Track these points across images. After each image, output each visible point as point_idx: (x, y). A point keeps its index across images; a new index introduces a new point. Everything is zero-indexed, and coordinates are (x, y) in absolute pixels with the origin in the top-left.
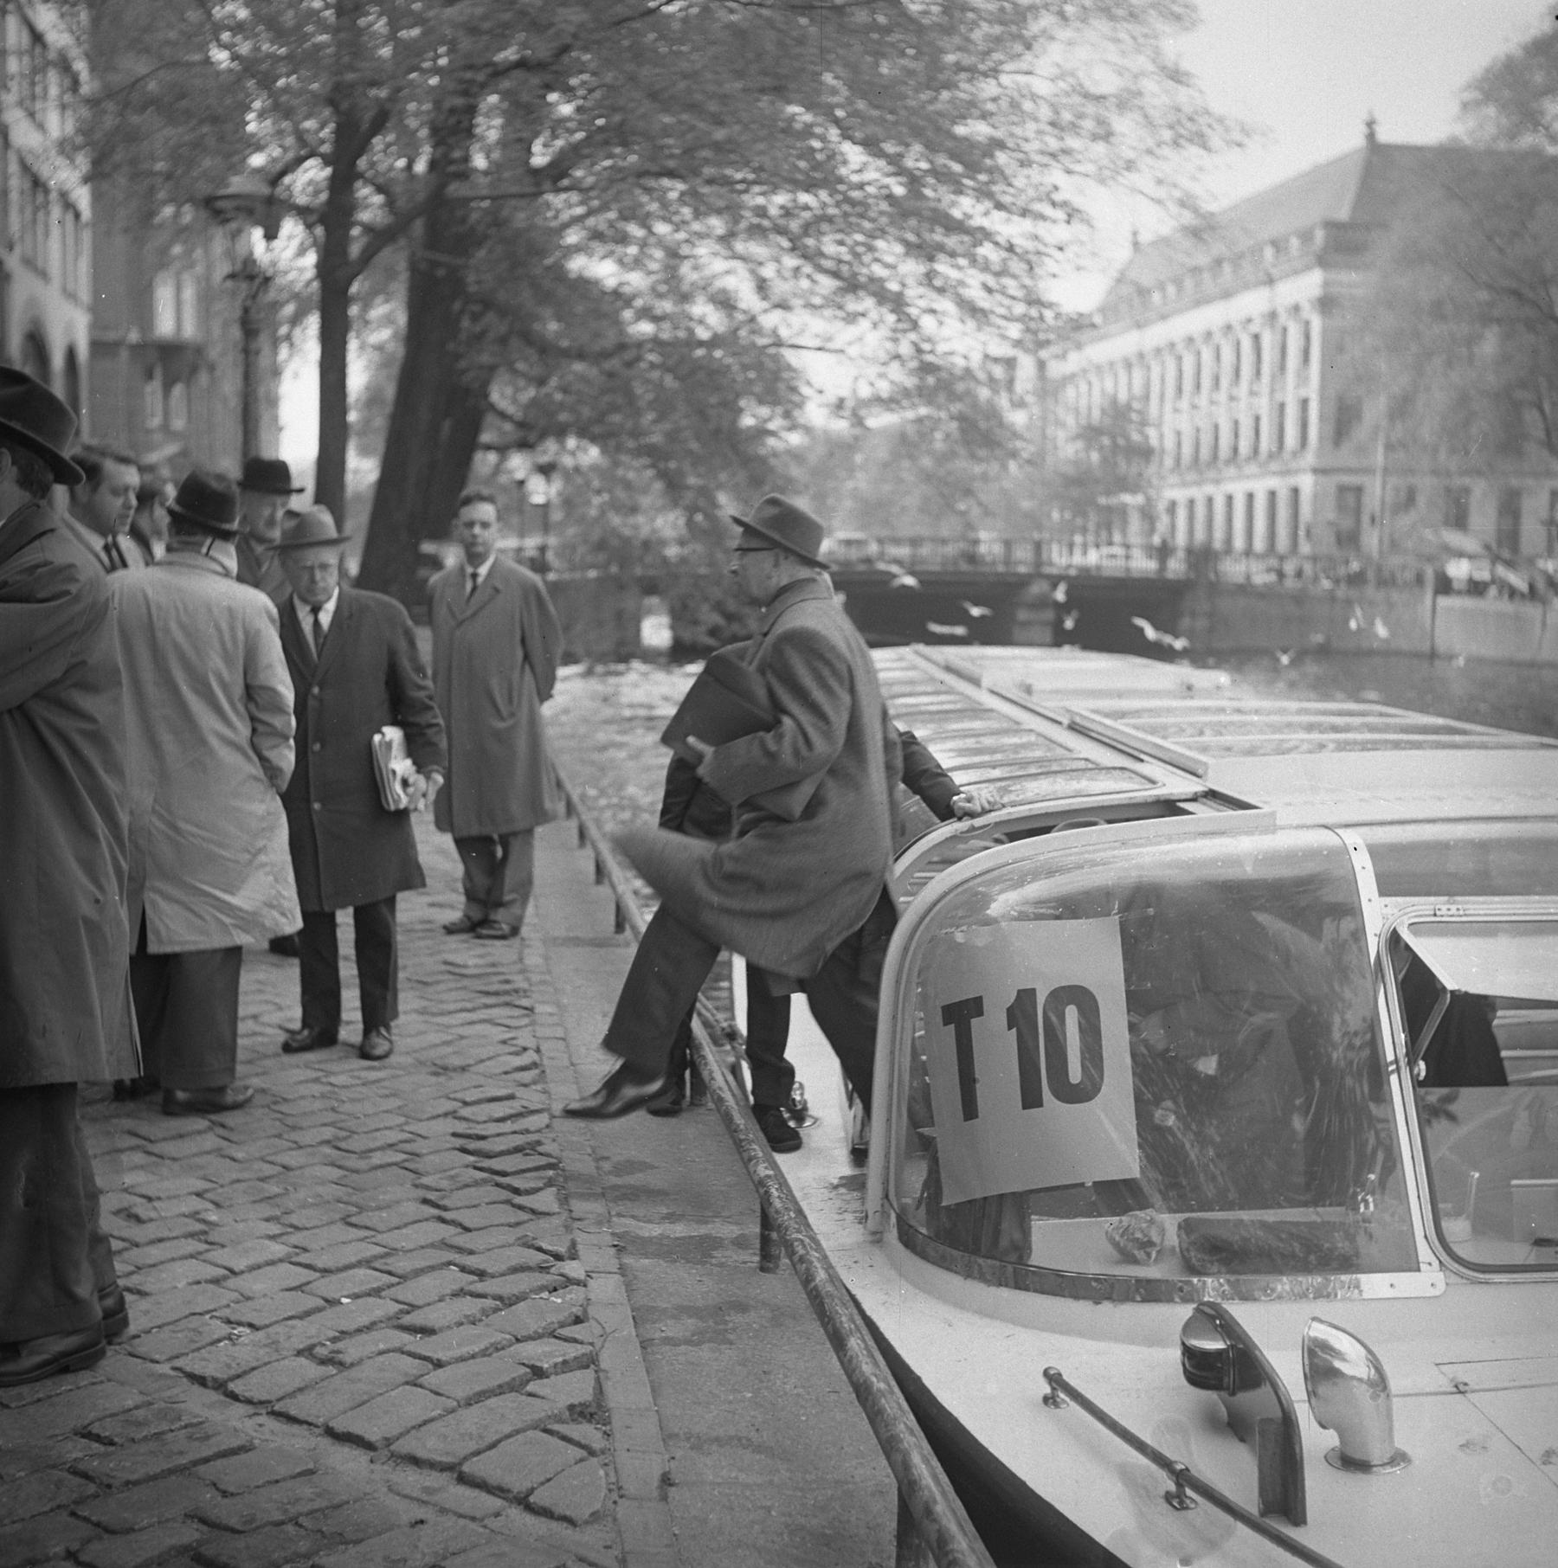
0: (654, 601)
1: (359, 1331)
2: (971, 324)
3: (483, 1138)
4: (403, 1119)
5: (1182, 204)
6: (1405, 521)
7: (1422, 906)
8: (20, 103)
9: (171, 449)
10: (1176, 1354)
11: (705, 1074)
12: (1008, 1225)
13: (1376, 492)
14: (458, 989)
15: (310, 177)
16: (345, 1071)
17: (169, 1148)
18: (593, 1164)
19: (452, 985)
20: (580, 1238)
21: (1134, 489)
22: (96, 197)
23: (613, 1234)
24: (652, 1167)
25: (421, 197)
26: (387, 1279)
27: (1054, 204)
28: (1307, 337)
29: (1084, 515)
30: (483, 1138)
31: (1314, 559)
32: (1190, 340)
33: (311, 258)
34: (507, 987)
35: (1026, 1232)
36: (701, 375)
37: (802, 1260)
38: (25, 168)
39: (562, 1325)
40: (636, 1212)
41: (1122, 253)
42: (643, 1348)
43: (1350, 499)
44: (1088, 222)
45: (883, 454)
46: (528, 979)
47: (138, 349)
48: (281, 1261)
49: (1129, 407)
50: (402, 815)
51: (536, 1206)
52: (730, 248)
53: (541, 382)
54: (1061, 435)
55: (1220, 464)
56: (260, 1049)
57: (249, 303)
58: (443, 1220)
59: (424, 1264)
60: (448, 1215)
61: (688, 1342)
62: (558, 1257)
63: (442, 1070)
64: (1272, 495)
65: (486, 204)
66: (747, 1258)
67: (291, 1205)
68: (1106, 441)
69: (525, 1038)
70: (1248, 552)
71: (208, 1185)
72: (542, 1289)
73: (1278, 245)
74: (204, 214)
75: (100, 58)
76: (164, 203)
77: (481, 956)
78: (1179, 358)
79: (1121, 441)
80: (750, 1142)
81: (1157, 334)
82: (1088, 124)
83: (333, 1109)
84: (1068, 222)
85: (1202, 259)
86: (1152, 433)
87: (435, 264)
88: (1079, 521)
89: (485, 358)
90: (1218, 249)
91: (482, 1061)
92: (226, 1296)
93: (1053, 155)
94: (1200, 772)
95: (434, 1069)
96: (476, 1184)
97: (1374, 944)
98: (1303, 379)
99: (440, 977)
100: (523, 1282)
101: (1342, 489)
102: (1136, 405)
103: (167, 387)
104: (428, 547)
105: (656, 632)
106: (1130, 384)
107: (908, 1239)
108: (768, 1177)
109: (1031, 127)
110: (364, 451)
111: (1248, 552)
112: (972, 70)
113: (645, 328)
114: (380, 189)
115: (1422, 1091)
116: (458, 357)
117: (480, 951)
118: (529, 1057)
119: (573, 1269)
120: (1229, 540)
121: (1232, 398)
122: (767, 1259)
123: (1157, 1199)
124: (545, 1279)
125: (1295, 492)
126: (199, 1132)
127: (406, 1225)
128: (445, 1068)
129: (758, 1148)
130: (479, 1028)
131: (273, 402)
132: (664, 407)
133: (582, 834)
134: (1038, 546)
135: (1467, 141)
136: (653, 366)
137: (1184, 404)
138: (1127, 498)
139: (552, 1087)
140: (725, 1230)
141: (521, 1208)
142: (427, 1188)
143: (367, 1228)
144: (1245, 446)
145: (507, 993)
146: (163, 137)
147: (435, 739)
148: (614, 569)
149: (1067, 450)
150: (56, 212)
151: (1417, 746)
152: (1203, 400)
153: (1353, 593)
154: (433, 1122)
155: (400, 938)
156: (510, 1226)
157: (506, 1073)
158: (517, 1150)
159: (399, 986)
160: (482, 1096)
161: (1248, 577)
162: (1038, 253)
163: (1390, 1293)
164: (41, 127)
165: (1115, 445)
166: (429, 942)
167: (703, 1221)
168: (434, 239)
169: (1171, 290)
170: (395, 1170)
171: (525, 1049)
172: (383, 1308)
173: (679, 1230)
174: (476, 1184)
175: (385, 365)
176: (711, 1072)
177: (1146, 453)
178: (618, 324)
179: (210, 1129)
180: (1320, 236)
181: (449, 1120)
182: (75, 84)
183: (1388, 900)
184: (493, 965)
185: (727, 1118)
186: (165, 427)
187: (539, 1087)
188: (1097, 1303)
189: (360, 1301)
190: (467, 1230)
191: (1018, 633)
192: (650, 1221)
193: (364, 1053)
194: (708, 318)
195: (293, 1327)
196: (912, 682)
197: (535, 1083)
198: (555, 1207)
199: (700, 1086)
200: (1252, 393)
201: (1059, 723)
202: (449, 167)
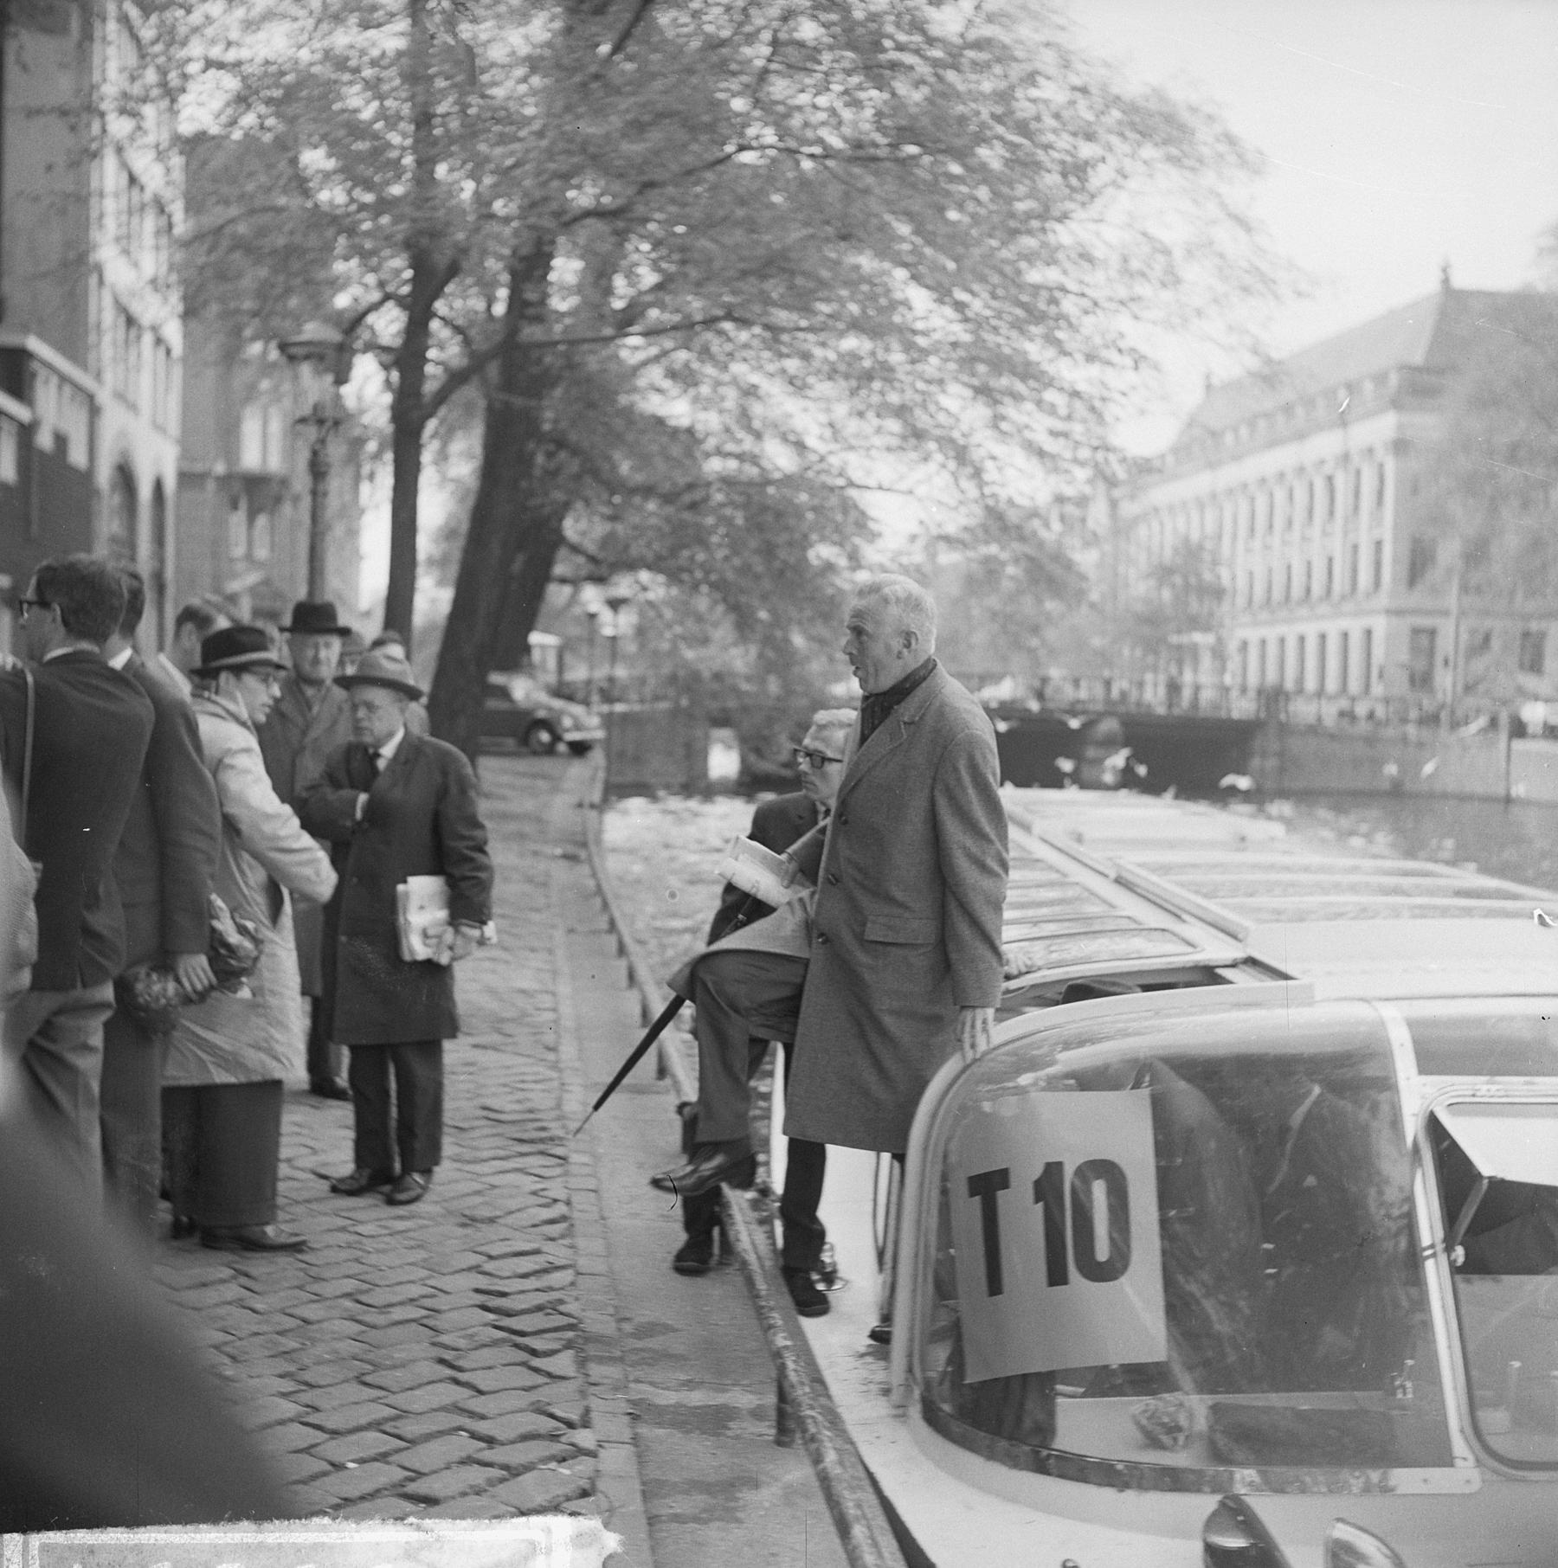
0: (725, 733)
1: (362, 1498)
3: (503, 1295)
4: (426, 1273)
5: (1255, 352)
6: (1479, 665)
7: (1461, 1085)
8: (118, 239)
9: (252, 578)
10: (1198, 1548)
11: (732, 1234)
12: (1032, 1404)
14: (494, 1135)
15: (388, 324)
18: (614, 1325)
19: (486, 1131)
20: (594, 1403)
21: (1207, 628)
24: (675, 1330)
25: (498, 338)
28: (1357, 493)
29: (1156, 653)
30: (503, 1295)
31: (1387, 701)
32: (1263, 481)
33: (388, 398)
34: (543, 1134)
35: (1051, 1414)
37: (813, 1439)
40: (657, 1378)
41: (1191, 397)
42: (650, 1524)
43: (1424, 641)
44: (1156, 367)
45: (955, 590)
46: (564, 1127)
47: (225, 481)
49: (1201, 547)
51: (551, 1369)
54: (1132, 573)
57: (317, 447)
58: (457, 1382)
59: (434, 1428)
60: (460, 1376)
62: (570, 1425)
63: (470, 1221)
67: (306, 1361)
68: (1178, 580)
69: (556, 1190)
70: (1320, 693)
72: (552, 1458)
73: (1351, 388)
74: (284, 360)
75: (194, 205)
76: (254, 339)
77: (519, 1102)
78: (1253, 500)
79: (1193, 580)
81: (1230, 475)
83: (357, 1260)
84: (1136, 368)
86: (1225, 574)
88: (1150, 659)
89: (558, 496)
91: (511, 1213)
93: (1122, 303)
96: (495, 1343)
98: (1377, 519)
99: (477, 1123)
101: (1416, 631)
102: (1209, 545)
104: (496, 678)
105: (723, 762)
106: (1202, 525)
107: (932, 1417)
108: (786, 1347)
111: (1320, 693)
114: (458, 330)
115: (1458, 1278)
118: (560, 1209)
119: (584, 1438)
120: (1300, 680)
124: (556, 1448)
125: (1368, 633)
126: (223, 1281)
127: (420, 1386)
128: (474, 1219)
130: (511, 1177)
133: (632, 977)
135: (1541, 288)
136: (722, 505)
137: (1257, 544)
138: (1198, 637)
139: (581, 1242)
140: (742, 1399)
141: (536, 1370)
142: (446, 1347)
144: (1317, 588)
145: (542, 1141)
148: (684, 702)
149: (1139, 588)
151: (1468, 912)
152: (1276, 541)
153: (1426, 734)
154: (457, 1276)
156: (524, 1389)
157: (534, 1226)
158: (539, 1308)
160: (508, 1250)
161: (1319, 719)
162: (1103, 399)
163: (1424, 1489)
164: (136, 265)
165: (1187, 585)
168: (508, 384)
169: (1244, 431)
170: (414, 1325)
171: (555, 1201)
172: (390, 1474)
174: (495, 1343)
176: (738, 1232)
177: (1218, 593)
179: (234, 1278)
180: (1394, 380)
181: (494, 1253)
184: (531, 1111)
185: (750, 1282)
186: (249, 557)
187: (566, 1242)
189: (366, 1466)
190: (481, 1392)
192: (668, 1389)
194: (781, 459)
197: (563, 1236)
198: (570, 1370)
199: (728, 1247)
200: (1325, 533)
201: (1106, 876)
202: (525, 307)
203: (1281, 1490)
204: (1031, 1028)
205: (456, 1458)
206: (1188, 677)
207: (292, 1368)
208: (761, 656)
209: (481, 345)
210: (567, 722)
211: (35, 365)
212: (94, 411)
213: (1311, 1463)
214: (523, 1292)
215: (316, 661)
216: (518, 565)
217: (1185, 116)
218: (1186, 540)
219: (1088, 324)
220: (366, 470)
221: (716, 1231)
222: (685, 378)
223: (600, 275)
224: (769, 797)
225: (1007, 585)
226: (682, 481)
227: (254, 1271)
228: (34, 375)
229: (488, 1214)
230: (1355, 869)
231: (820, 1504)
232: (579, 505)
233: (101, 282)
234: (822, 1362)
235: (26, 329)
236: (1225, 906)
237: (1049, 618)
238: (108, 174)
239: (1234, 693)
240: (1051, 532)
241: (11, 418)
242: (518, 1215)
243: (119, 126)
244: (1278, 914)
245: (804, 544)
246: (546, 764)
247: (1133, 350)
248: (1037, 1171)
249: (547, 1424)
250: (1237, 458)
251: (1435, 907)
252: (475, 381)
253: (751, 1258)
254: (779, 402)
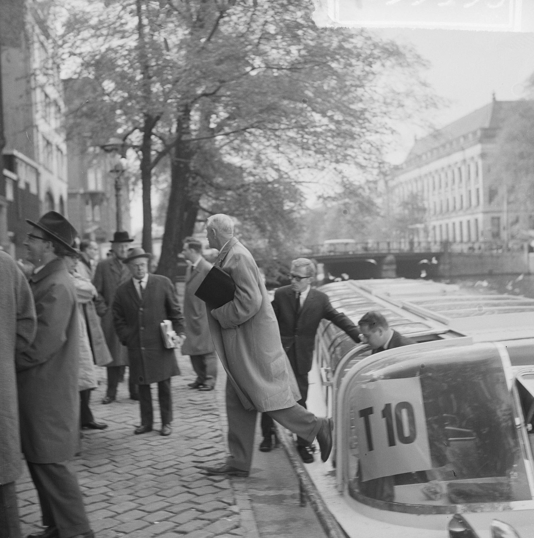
2: (361, 171)
5: (430, 127)
9: (95, 227)
11: (278, 436)
12: (386, 488)
13: (505, 219)
15: (136, 137)
16: (155, 440)
17: (96, 470)
19: (193, 408)
20: (237, 497)
21: (421, 222)
22: (68, 146)
23: (249, 495)
24: (262, 471)
26: (171, 514)
27: (386, 129)
30: (202, 462)
31: (485, 243)
33: (138, 163)
36: (270, 193)
38: (44, 138)
39: (232, 529)
41: (411, 144)
43: (496, 221)
47: (84, 195)
48: (134, 509)
49: (417, 195)
50: (172, 350)
52: (278, 150)
53: (217, 199)
56: (127, 433)
60: (191, 491)
61: (275, 533)
62: (230, 504)
63: (189, 438)
64: (469, 222)
65: (196, 142)
66: (295, 502)
68: (410, 206)
69: (217, 427)
70: (462, 242)
71: (110, 483)
73: (465, 137)
74: (103, 151)
75: (68, 101)
77: (201, 397)
78: (433, 177)
80: (296, 460)
81: (425, 169)
82: (395, 103)
83: (151, 454)
85: (437, 144)
87: (179, 162)
88: (402, 234)
89: (198, 192)
90: (443, 141)
91: (202, 435)
92: (115, 522)
93: (385, 113)
94: (446, 323)
95: (186, 438)
96: (201, 479)
97: (510, 384)
98: (477, 182)
100: (219, 514)
101: (493, 218)
102: (420, 194)
103: (93, 206)
106: (417, 186)
107: (352, 494)
109: (377, 105)
110: (159, 225)
111: (462, 242)
112: (357, 86)
113: (251, 179)
114: (161, 138)
116: (188, 192)
117: (201, 395)
119: (235, 508)
120: (454, 238)
121: (452, 190)
122: (303, 503)
123: (439, 477)
125: (476, 220)
126: (106, 464)
128: (190, 438)
129: (298, 461)
131: (128, 209)
132: (258, 205)
134: (389, 244)
135: (527, 99)
136: (254, 191)
138: (418, 226)
140: (288, 492)
143: (163, 496)
144: (458, 206)
146: (88, 124)
147: (182, 323)
149: (397, 210)
150: (55, 152)
151: (522, 311)
152: (443, 190)
155: (173, 392)
159: (174, 409)
160: (202, 447)
164: (49, 124)
165: (413, 208)
166: (184, 393)
167: (279, 489)
168: (178, 154)
169: (429, 154)
172: (169, 525)
173: (272, 493)
175: (165, 195)
177: (424, 210)
178: (241, 177)
180: (479, 133)
181: (198, 448)
182: (59, 110)
183: (515, 367)
186: (93, 221)
188: (419, 515)
189: (162, 523)
190: (198, 496)
191: (384, 274)
193: (162, 433)
194: (272, 175)
195: (139, 533)
196: (348, 294)
199: (278, 441)
200: (459, 187)
202: (183, 129)
203: (474, 511)
204: (377, 359)
205: (192, 518)
206: (416, 240)
207: (132, 491)
208: (269, 242)
209: (169, 143)
211: (17, 160)
212: (38, 174)
213: (484, 501)
214: (208, 461)
215: (123, 252)
216: (186, 214)
217: (401, 50)
218: (412, 193)
219: (374, 120)
220: (131, 187)
221: (273, 437)
222: (237, 150)
224: (276, 289)
225: (352, 211)
226: (239, 184)
227: (116, 460)
228: (17, 164)
229: (195, 435)
230: (477, 299)
231: (318, 526)
232: (204, 195)
233: (38, 131)
234: (313, 478)
235: (12, 148)
236: (440, 313)
237: (367, 222)
238: (38, 96)
239: (432, 244)
240: (366, 193)
241: (10, 178)
242: (205, 435)
243: (41, 79)
244: (459, 315)
245: (281, 203)
247: (390, 128)
248: (382, 407)
249: (222, 505)
250: (427, 163)
251: (512, 309)
252: (168, 155)
253: (286, 444)
254: (272, 155)
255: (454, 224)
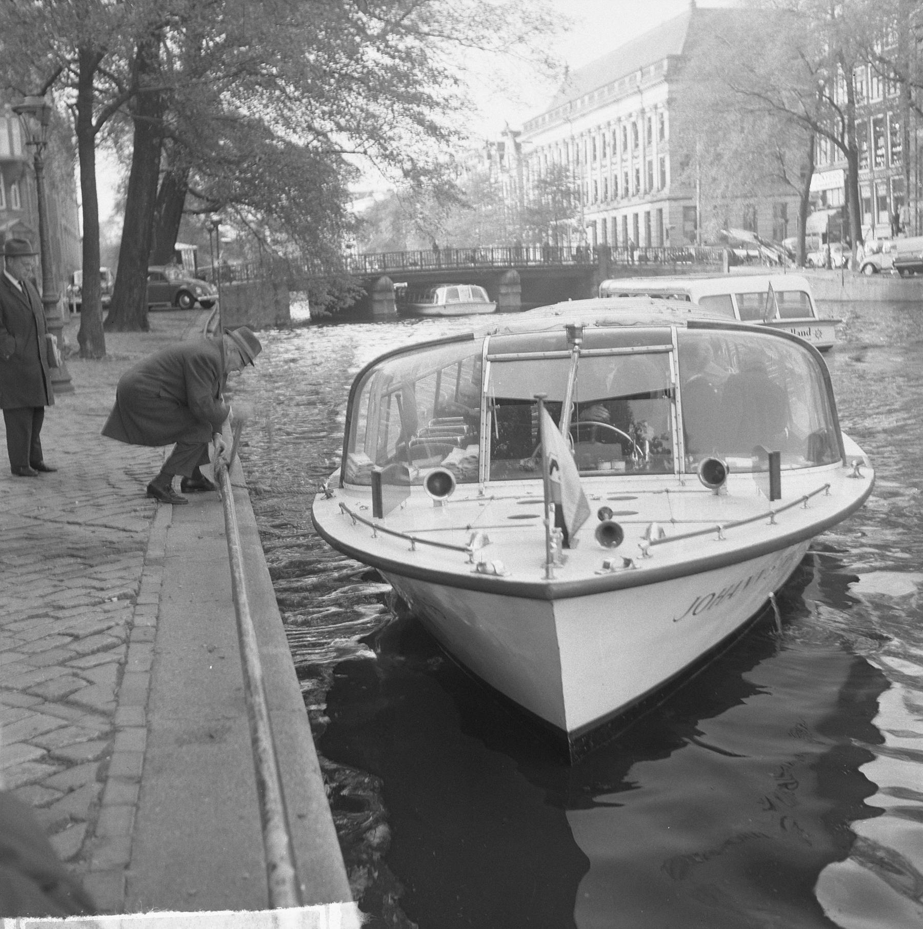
55: (619, 198)
81: (579, 126)
105: (300, 311)
125: (660, 211)
177: (578, 195)
180: (665, 63)
186: (9, 209)
210: (199, 291)
223: (194, 40)
246: (188, 314)
255: (625, 217)
